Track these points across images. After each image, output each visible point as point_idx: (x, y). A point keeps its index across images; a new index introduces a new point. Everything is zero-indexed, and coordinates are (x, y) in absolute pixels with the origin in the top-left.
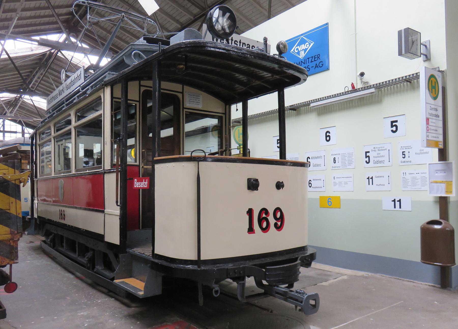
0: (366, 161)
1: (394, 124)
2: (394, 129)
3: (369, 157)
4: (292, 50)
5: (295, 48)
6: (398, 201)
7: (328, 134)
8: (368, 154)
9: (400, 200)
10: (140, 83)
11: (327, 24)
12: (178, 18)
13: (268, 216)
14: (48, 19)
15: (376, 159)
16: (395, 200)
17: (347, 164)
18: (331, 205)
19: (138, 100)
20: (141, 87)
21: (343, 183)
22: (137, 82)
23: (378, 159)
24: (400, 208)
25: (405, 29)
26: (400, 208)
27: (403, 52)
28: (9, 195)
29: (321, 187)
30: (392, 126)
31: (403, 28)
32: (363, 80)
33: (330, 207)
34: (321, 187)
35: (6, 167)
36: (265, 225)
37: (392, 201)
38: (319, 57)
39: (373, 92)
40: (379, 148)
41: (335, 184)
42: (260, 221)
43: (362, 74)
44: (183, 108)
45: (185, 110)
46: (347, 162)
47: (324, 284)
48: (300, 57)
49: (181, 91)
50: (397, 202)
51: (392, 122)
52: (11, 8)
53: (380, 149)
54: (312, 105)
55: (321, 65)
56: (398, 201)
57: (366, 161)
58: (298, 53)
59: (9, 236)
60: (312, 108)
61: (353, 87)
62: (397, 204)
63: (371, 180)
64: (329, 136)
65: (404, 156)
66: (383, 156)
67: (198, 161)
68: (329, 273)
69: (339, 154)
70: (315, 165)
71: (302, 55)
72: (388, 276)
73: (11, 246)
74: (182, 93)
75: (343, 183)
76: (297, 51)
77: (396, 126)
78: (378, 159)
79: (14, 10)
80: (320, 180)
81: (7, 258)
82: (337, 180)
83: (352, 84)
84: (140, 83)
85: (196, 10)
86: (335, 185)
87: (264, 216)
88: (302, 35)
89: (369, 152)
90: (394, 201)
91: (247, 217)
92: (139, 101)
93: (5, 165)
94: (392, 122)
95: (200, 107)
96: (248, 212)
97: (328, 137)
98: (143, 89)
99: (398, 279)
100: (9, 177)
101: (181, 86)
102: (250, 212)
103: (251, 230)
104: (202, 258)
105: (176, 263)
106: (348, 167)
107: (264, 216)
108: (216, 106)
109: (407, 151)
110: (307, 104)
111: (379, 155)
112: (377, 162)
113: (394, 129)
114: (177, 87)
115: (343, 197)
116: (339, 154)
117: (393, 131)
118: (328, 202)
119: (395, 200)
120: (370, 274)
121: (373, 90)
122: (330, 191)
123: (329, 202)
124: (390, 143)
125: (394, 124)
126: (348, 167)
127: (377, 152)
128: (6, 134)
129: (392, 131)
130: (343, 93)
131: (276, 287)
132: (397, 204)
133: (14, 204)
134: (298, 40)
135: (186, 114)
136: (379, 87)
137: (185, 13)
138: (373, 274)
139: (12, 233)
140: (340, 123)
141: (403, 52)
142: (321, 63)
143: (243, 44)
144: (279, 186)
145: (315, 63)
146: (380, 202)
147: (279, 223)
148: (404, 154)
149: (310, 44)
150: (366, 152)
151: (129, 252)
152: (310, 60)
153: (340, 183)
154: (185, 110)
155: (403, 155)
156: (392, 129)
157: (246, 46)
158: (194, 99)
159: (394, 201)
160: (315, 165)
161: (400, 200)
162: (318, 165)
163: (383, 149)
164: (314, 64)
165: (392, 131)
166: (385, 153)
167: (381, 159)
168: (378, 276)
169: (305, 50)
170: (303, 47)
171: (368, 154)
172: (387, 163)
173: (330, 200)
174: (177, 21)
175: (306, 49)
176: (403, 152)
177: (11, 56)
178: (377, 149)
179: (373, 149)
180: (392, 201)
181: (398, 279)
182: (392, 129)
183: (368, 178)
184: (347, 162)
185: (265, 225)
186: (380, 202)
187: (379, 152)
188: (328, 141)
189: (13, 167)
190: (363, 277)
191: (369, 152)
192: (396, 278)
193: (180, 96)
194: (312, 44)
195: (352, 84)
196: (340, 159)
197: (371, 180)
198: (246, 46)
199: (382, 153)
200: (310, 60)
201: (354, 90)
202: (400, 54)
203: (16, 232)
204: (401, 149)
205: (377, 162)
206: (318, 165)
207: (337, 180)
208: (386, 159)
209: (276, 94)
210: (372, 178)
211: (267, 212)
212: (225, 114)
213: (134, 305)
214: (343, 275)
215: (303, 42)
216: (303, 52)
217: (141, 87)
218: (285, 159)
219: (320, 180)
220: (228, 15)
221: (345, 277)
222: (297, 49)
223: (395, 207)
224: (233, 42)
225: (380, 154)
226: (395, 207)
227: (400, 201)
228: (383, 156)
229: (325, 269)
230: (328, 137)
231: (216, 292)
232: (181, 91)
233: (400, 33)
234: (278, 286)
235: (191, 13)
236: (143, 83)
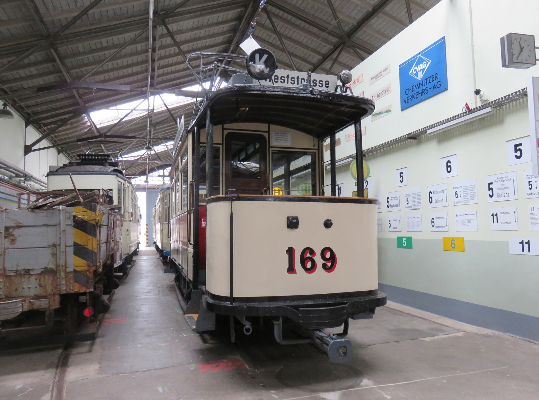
0: (490, 195)
1: (518, 148)
2: (518, 154)
3: (492, 189)
4: (411, 72)
5: (413, 69)
6: (526, 243)
7: (449, 164)
8: (491, 186)
9: (529, 241)
10: (223, 127)
11: (444, 38)
12: (318, 49)
13: (315, 255)
14: (185, 72)
15: (500, 192)
16: (523, 241)
17: (469, 199)
18: (454, 248)
19: (221, 143)
20: (225, 131)
21: (466, 221)
22: (221, 126)
23: (502, 191)
24: (529, 251)
25: (507, 35)
26: (529, 251)
27: (507, 63)
28: (86, 232)
29: (444, 227)
30: (516, 151)
31: (505, 34)
32: (483, 98)
33: (454, 250)
34: (444, 227)
35: (85, 210)
36: (309, 265)
37: (520, 243)
38: (436, 76)
39: (490, 112)
40: (503, 178)
41: (458, 222)
42: (303, 261)
43: (478, 92)
44: (270, 147)
45: (271, 149)
46: (469, 197)
47: (427, 339)
48: (418, 78)
49: (267, 130)
50: (525, 244)
51: (516, 146)
52: (165, 64)
53: (504, 179)
54: (428, 132)
55: (439, 86)
56: (526, 243)
57: (490, 195)
58: (416, 74)
59: (86, 268)
60: (429, 135)
61: (468, 108)
62: (526, 246)
63: (495, 217)
64: (450, 166)
65: (530, 187)
66: (507, 188)
67: (232, 201)
68: (445, 328)
69: (461, 187)
70: (437, 201)
71: (420, 76)
72: (518, 337)
73: (87, 276)
74: (268, 132)
75: (466, 221)
76: (414, 73)
77: (520, 150)
78: (502, 191)
79: (198, 58)
80: (443, 218)
81: (84, 286)
82: (460, 218)
83: (467, 104)
84: (223, 127)
85: (335, 40)
86: (458, 224)
87: (308, 255)
88: (419, 53)
89: (491, 183)
90: (522, 243)
91: (287, 256)
92: (222, 144)
93: (85, 208)
94: (516, 146)
95: (288, 144)
96: (287, 252)
97: (449, 168)
98: (226, 132)
99: (530, 341)
100: (86, 218)
101: (267, 125)
102: (290, 252)
103: (291, 269)
104: (234, 296)
105: (223, 301)
106: (471, 202)
107: (308, 255)
108: (304, 141)
109: (533, 181)
110: (423, 131)
111: (503, 187)
112: (500, 196)
113: (518, 154)
114: (262, 127)
115: (467, 237)
116: (461, 187)
117: (517, 157)
118: (452, 244)
119: (523, 241)
120: (497, 333)
121: (489, 109)
122: (454, 231)
123: (453, 244)
124: (515, 172)
125: (518, 148)
126: (471, 202)
127: (501, 183)
128: (165, 178)
129: (516, 157)
130: (460, 114)
131: (318, 333)
132: (526, 246)
133: (91, 239)
134: (415, 60)
135: (272, 153)
136: (498, 105)
137: (325, 44)
138: (500, 333)
139: (88, 266)
140: (461, 150)
141: (507, 63)
142: (439, 83)
143: (302, 79)
144: (328, 224)
145: (433, 83)
146: (505, 244)
147: (329, 264)
148: (531, 185)
149: (427, 63)
150: (489, 184)
151: (200, 289)
152: (428, 80)
153: (463, 221)
154: (271, 149)
155: (529, 185)
156: (516, 154)
157: (306, 81)
158: (282, 138)
159: (522, 243)
160: (437, 201)
161: (529, 241)
162: (440, 201)
163: (507, 179)
164: (431, 85)
165: (516, 157)
166: (509, 184)
167: (505, 191)
168: (507, 336)
169: (423, 70)
170: (421, 67)
171: (491, 186)
172: (512, 196)
173: (453, 242)
174: (319, 53)
175: (424, 69)
176: (529, 182)
177: (169, 107)
178: (500, 180)
179: (497, 180)
180: (520, 243)
181: (530, 341)
182: (516, 154)
183: (493, 215)
184: (469, 197)
185: (309, 265)
186: (505, 244)
187: (503, 183)
188: (449, 172)
189: (91, 210)
190: (487, 336)
191: (491, 183)
192: (527, 341)
193: (266, 135)
194: (429, 63)
195: (467, 104)
196: (462, 193)
197: (495, 217)
198: (306, 81)
199: (506, 184)
200: (428, 80)
201: (469, 110)
202: (504, 65)
203: (92, 265)
204: (527, 178)
205: (500, 196)
206: (440, 201)
207: (460, 218)
208: (511, 191)
209: (353, 127)
210: (496, 215)
211: (312, 252)
212: (318, 149)
213: (211, 342)
214: (459, 331)
215: (420, 61)
216: (421, 73)
217: (225, 131)
218: (363, 196)
219: (443, 218)
220: (265, 56)
221: (460, 334)
222: (415, 70)
223: (523, 251)
224: (290, 79)
225: (504, 185)
226: (523, 251)
227: (528, 243)
228: (507, 188)
229: (445, 324)
230: (449, 168)
231: (248, 330)
232: (267, 130)
233: (502, 40)
234: (320, 331)
235: (329, 42)
236: (226, 126)
